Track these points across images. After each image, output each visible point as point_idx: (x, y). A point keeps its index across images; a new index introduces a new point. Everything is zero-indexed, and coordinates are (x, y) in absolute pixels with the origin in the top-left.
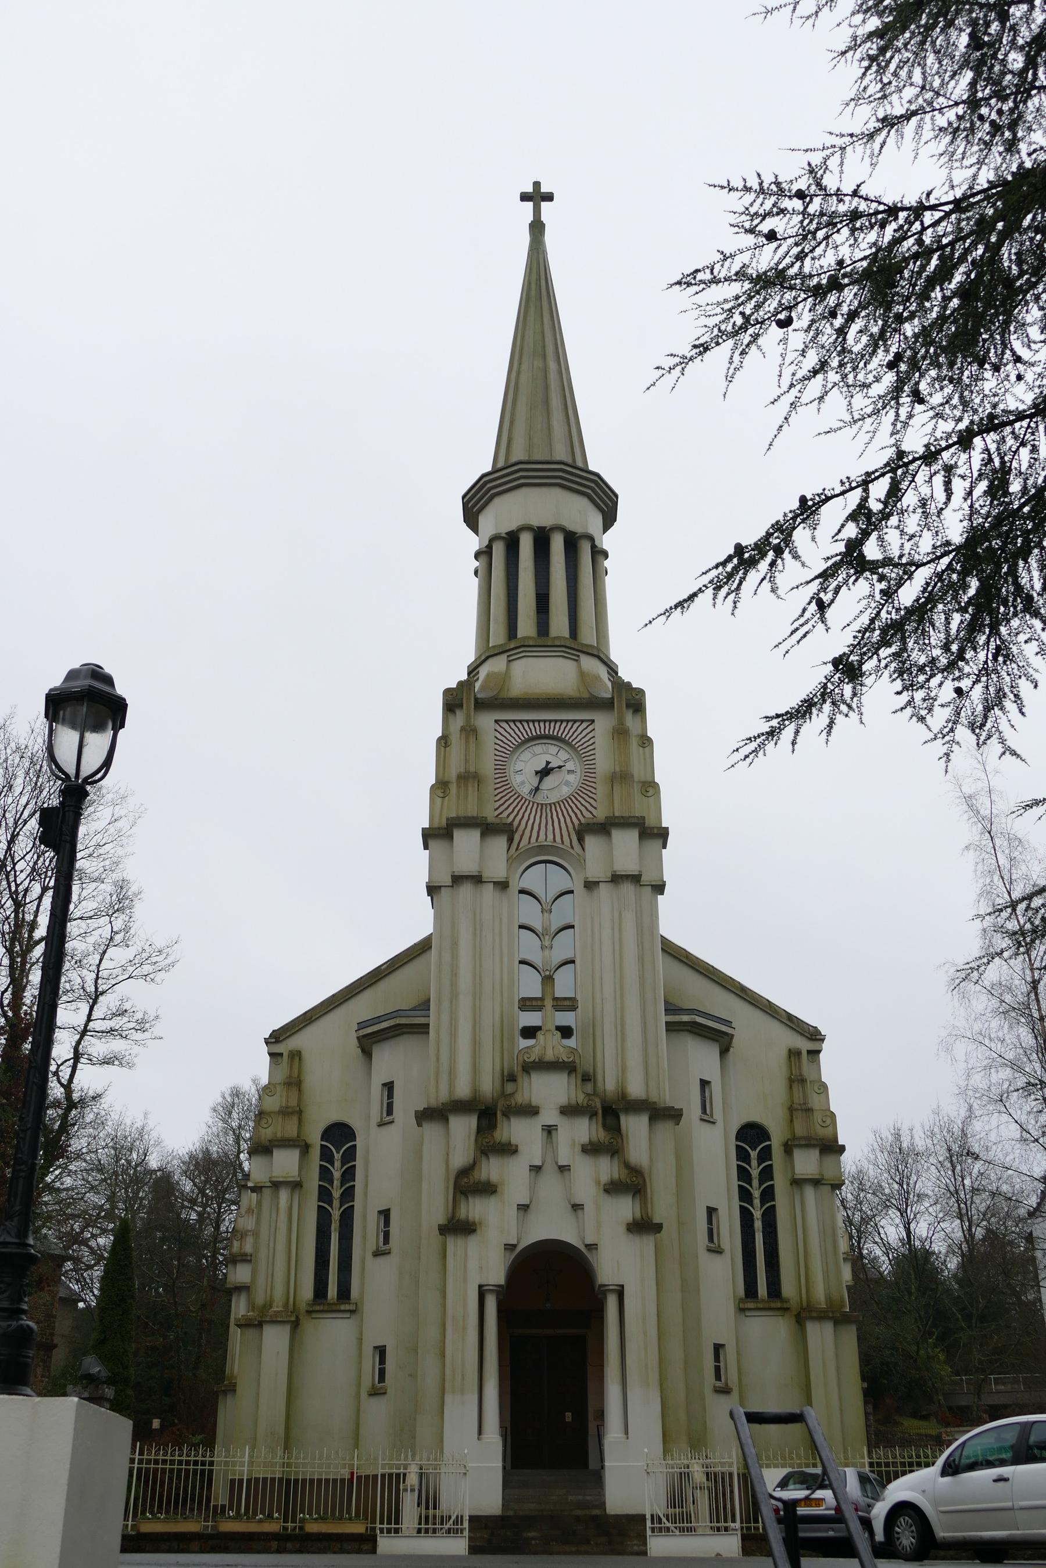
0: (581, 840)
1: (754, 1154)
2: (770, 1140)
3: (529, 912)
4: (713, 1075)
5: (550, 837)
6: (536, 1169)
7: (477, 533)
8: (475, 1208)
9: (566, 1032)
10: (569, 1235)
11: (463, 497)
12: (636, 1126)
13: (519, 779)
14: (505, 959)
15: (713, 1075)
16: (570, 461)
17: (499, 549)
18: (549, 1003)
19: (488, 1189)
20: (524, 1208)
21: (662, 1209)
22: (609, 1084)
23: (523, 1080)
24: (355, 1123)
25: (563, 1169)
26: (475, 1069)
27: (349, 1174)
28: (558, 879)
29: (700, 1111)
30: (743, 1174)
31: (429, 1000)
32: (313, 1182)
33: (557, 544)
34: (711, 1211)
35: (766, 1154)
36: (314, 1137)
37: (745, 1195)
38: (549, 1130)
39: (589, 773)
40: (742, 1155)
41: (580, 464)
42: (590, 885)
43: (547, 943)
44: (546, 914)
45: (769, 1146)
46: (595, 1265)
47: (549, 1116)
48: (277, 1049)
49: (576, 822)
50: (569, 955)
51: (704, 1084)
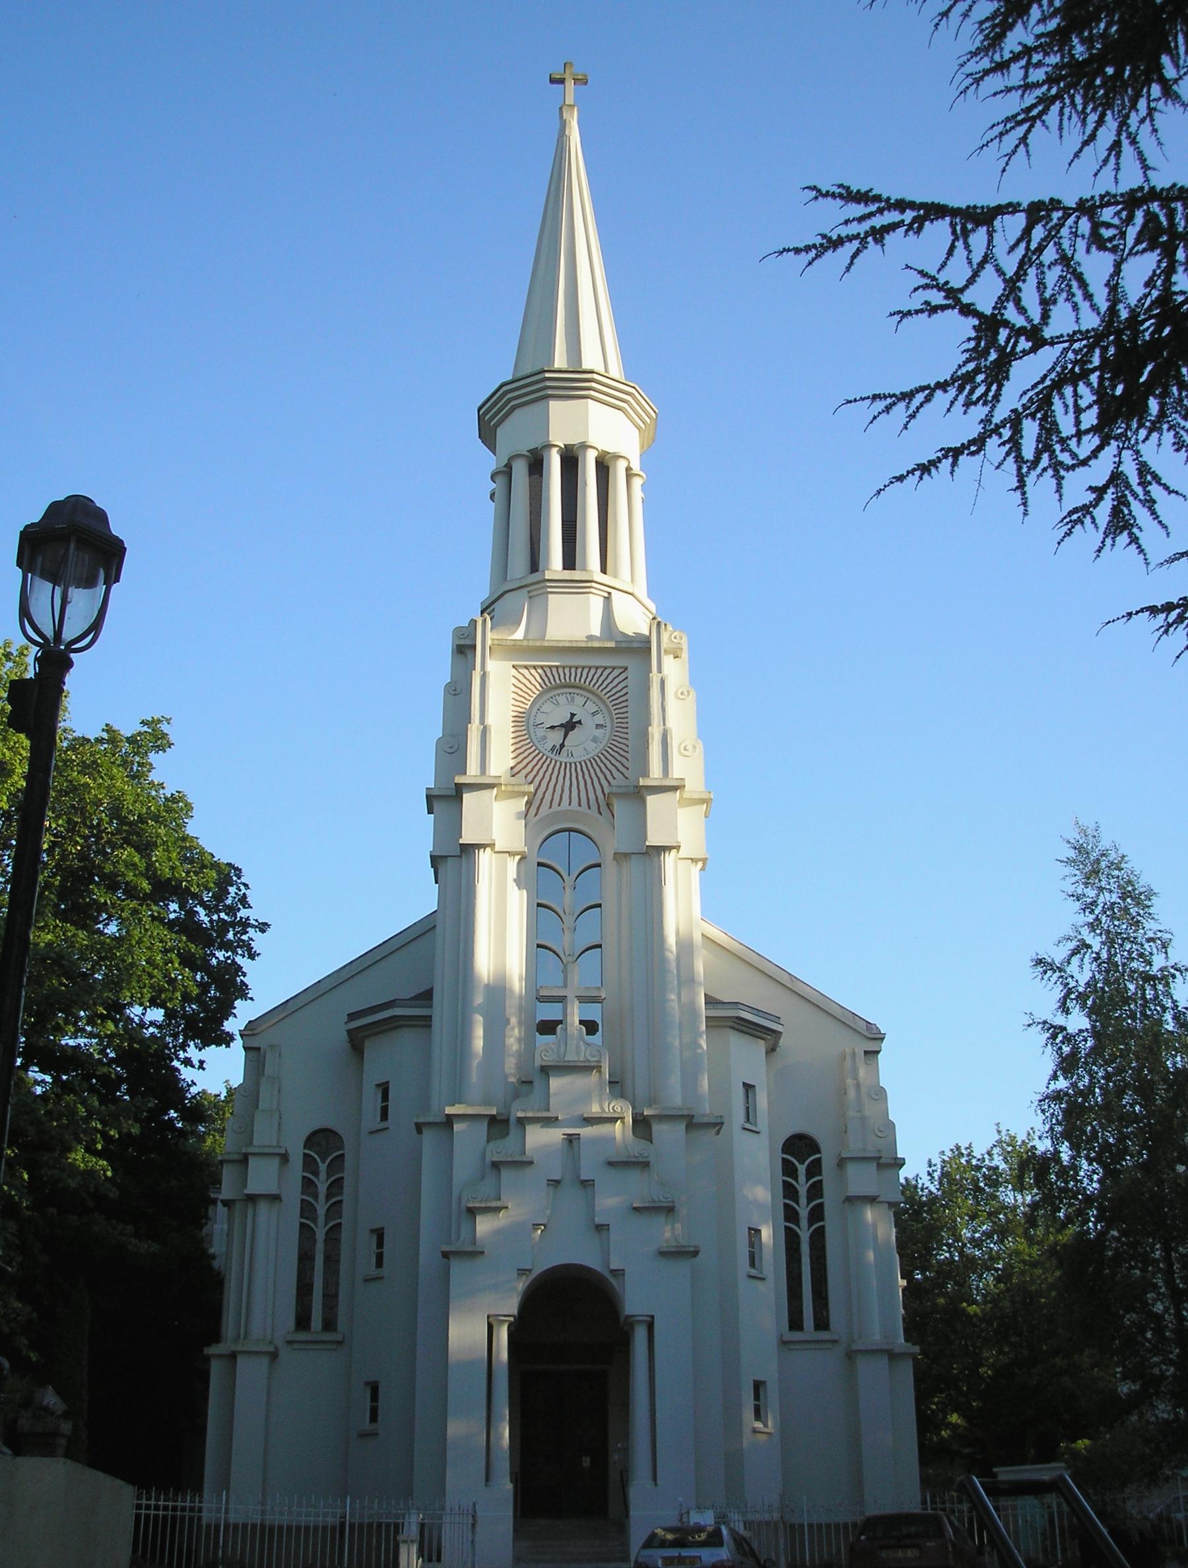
1: (802, 1169)
2: (818, 1151)
6: (555, 1183)
17: (520, 470)
25: (587, 1184)
27: (336, 1186)
30: (790, 1191)
34: (758, 1386)
40: (789, 1170)
51: (748, 1088)
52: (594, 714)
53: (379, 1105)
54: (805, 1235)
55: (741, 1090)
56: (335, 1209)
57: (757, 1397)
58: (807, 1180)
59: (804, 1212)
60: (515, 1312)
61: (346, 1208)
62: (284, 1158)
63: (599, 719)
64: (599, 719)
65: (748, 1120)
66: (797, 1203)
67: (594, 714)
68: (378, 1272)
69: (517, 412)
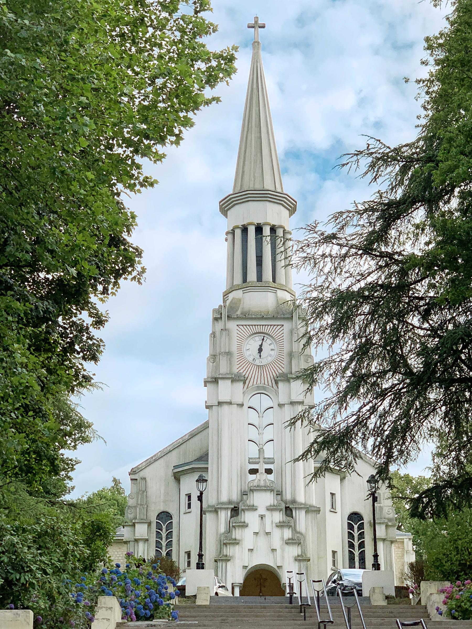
0: (276, 383)
1: (356, 527)
2: (363, 520)
3: (253, 416)
4: (337, 490)
5: (263, 382)
6: (256, 534)
7: (227, 217)
8: (229, 551)
9: (269, 471)
10: (271, 563)
11: (220, 202)
12: (300, 516)
13: (248, 353)
14: (278, 201)
15: (337, 490)
16: (273, 189)
17: (238, 233)
18: (261, 460)
19: (236, 542)
20: (251, 550)
21: (311, 552)
22: (288, 497)
23: (251, 495)
24: (172, 511)
25: (268, 534)
26: (230, 491)
27: (170, 535)
28: (266, 402)
29: (330, 507)
30: (351, 535)
31: (207, 455)
32: (153, 539)
33: (267, 231)
34: (334, 553)
35: (361, 527)
36: (154, 519)
37: (351, 545)
38: (262, 517)
39: (281, 351)
40: (350, 527)
41: (279, 190)
42: (281, 406)
43: (260, 432)
44: (261, 418)
45: (363, 523)
46: (281, 574)
47: (262, 510)
48: (134, 477)
49: (275, 375)
50: (271, 438)
51: (332, 494)
52: (270, 345)
53: (187, 502)
54: (357, 553)
55: (330, 496)
56: (169, 544)
57: (334, 557)
58: (358, 531)
59: (356, 544)
60: (242, 582)
61: (174, 534)
62: (149, 524)
63: (272, 347)
64: (272, 347)
65: (332, 508)
66: (354, 540)
67: (270, 345)
68: (189, 510)
69: (237, 207)
